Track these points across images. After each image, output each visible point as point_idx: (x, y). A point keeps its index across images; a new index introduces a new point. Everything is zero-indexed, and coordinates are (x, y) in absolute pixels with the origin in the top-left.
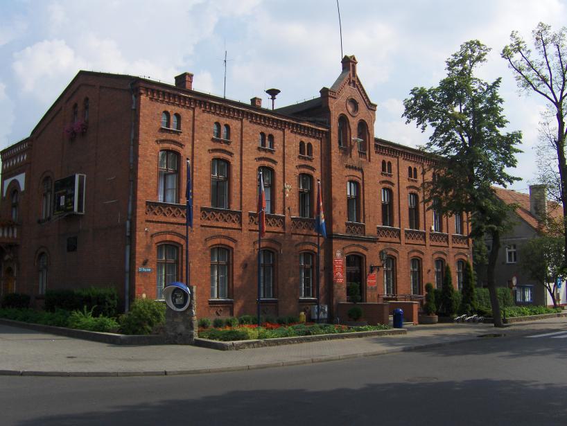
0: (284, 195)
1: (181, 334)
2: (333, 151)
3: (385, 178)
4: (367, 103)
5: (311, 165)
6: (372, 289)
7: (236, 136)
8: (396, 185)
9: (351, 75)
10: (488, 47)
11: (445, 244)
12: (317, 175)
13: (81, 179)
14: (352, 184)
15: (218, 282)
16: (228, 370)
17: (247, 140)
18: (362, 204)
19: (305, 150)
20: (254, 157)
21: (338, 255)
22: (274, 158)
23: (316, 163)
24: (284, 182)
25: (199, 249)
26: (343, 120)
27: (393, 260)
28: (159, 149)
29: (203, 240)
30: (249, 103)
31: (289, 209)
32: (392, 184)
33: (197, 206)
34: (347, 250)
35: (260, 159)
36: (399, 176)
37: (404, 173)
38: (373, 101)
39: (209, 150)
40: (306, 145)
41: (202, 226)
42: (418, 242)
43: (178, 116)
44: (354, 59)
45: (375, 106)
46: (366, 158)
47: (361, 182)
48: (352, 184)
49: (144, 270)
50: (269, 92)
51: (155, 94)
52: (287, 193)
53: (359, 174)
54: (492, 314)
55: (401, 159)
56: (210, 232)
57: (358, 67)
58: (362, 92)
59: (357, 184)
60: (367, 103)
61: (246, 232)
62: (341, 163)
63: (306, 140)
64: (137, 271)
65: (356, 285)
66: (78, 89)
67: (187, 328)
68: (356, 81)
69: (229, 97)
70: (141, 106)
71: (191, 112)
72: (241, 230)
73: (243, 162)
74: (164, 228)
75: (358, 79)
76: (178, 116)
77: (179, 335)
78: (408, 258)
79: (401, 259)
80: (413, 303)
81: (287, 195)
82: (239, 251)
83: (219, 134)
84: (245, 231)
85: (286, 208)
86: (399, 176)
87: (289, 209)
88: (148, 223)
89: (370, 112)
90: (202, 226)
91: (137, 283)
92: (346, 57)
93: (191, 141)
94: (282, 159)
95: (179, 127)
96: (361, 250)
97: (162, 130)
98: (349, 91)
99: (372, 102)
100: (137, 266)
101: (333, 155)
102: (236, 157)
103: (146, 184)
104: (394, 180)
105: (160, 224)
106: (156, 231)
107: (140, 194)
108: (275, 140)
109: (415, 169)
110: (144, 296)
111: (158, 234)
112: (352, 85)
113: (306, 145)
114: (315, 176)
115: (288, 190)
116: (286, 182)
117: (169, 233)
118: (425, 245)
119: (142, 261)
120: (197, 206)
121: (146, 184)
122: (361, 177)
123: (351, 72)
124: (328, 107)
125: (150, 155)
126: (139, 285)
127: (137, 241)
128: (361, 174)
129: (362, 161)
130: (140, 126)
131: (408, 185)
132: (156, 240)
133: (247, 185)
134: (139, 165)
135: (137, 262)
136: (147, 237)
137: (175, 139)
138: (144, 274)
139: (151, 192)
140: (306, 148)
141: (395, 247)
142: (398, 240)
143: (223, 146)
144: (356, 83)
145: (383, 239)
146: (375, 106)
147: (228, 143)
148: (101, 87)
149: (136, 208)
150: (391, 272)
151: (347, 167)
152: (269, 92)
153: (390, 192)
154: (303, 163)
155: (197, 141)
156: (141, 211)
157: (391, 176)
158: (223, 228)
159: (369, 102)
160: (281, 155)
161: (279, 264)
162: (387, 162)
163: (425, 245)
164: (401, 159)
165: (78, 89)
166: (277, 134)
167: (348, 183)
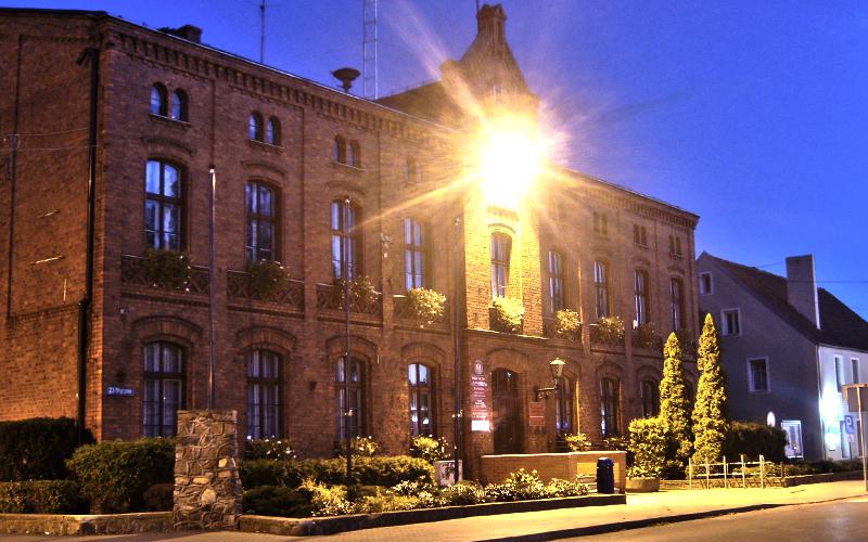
6: (537, 431)
9: (496, 42)
15: (413, 273)
16: (183, 536)
21: (479, 368)
25: (225, 352)
28: (145, 156)
31: (389, 281)
39: (242, 162)
41: (230, 308)
43: (182, 94)
50: (338, 74)
52: (386, 250)
61: (311, 320)
65: (688, 366)
72: (303, 317)
76: (182, 94)
77: (203, 509)
82: (300, 358)
83: (260, 134)
87: (389, 281)
92: (486, 7)
95: (184, 115)
102: (293, 180)
103: (122, 221)
108: (363, 151)
121: (122, 221)
123: (496, 36)
125: (130, 167)
143: (268, 157)
147: (277, 152)
148: (22, 38)
152: (338, 74)
158: (269, 313)
161: (373, 384)
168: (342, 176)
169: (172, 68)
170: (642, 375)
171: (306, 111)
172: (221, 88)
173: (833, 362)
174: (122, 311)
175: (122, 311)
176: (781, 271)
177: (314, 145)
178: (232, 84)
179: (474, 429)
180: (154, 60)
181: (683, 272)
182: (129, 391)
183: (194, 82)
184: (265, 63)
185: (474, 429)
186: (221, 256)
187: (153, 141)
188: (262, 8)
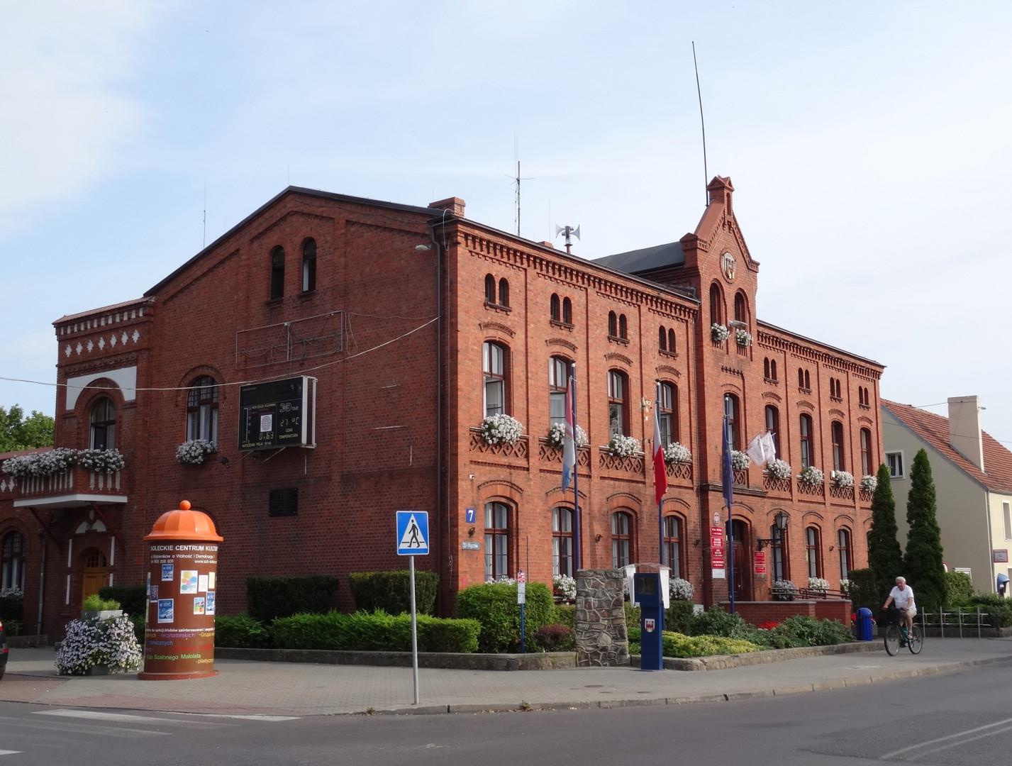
0: (643, 418)
1: (604, 649)
2: (704, 344)
3: (614, 348)
4: (747, 259)
5: (674, 367)
7: (579, 318)
8: (784, 401)
11: (850, 502)
12: (682, 384)
13: (310, 382)
14: (558, 364)
17: (595, 325)
18: (743, 433)
19: (667, 341)
20: (603, 354)
22: (508, 324)
23: (682, 363)
24: (642, 396)
25: (538, 510)
26: (716, 289)
27: (629, 516)
29: (543, 494)
32: (779, 399)
33: (534, 438)
35: (611, 356)
36: (786, 385)
37: (652, 339)
39: (546, 341)
40: (667, 332)
44: (730, 184)
45: (758, 264)
46: (745, 354)
47: (741, 396)
48: (558, 364)
49: (470, 546)
53: (737, 381)
54: (639, 636)
55: (644, 309)
57: (735, 197)
58: (739, 241)
59: (734, 397)
62: (716, 364)
63: (668, 323)
64: (460, 548)
66: (283, 219)
67: (614, 639)
68: (733, 221)
69: (526, 235)
70: (459, 265)
71: (522, 274)
73: (590, 361)
75: (734, 218)
78: (803, 527)
80: (807, 605)
81: (647, 418)
84: (595, 479)
85: (646, 441)
86: (786, 385)
88: (473, 466)
89: (751, 273)
90: (541, 471)
91: (460, 569)
93: (524, 326)
94: (638, 356)
96: (745, 512)
98: (723, 237)
99: (754, 258)
100: (460, 540)
101: (705, 349)
102: (520, 335)
104: (781, 393)
105: (488, 468)
106: (484, 479)
107: (462, 417)
109: (671, 331)
112: (727, 227)
113: (667, 332)
114: (679, 386)
115: (647, 410)
116: (645, 396)
118: (825, 504)
119: (467, 530)
120: (534, 438)
122: (741, 388)
123: (725, 206)
124: (696, 268)
125: (472, 350)
126: (462, 572)
127: (460, 497)
128: (741, 381)
129: (741, 360)
130: (459, 299)
131: (798, 400)
133: (597, 401)
134: (459, 366)
135: (460, 533)
136: (472, 490)
137: (503, 323)
138: (470, 552)
139: (475, 413)
140: (561, 304)
142: (522, 463)
144: (731, 225)
145: (775, 493)
146: (758, 264)
149: (457, 440)
151: (724, 369)
153: (504, 348)
154: (664, 364)
155: (531, 326)
156: (464, 444)
157: (809, 392)
160: (637, 349)
162: (618, 314)
163: (644, 483)
164: (644, 309)
165: (283, 219)
166: (631, 313)
167: (552, 360)
168: (615, 348)
169: (477, 254)
170: (839, 524)
171: (589, 290)
172: (531, 275)
173: (996, 502)
174: (471, 476)
175: (471, 476)
176: (943, 412)
177: (595, 321)
178: (539, 271)
179: (181, 593)
180: (486, 255)
181: (871, 422)
182: (476, 546)
183: (512, 272)
184: (521, 236)
185: (181, 593)
186: (534, 425)
187: (487, 326)
188: (518, 181)
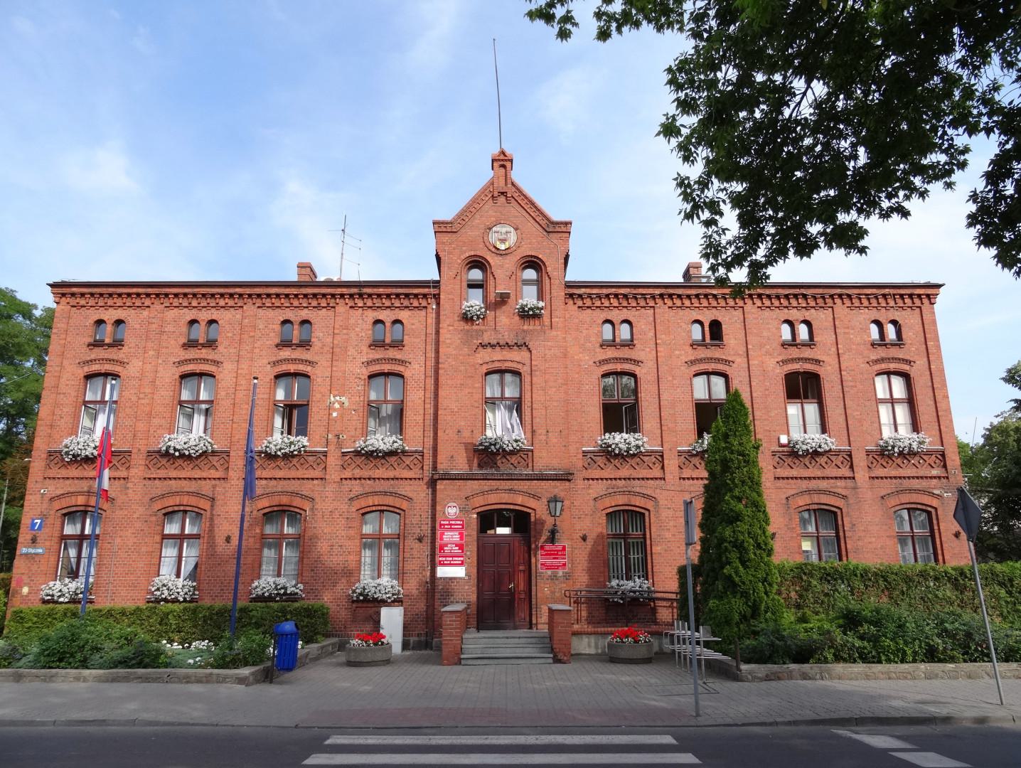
10: (577, 21)
20: (266, 361)
29: (147, 499)
30: (293, 276)
34: (479, 501)
35: (785, 362)
38: (556, 216)
42: (840, 473)
49: (32, 551)
51: (791, 301)
56: (160, 488)
60: (543, 223)
74: (804, 485)
79: (665, 514)
97: (784, 345)
110: (25, 590)
111: (59, 497)
117: (375, 493)
122: (528, 362)
132: (57, 505)
137: (398, 357)
141: (649, 488)
143: (894, 352)
150: (930, 538)
159: (548, 219)
